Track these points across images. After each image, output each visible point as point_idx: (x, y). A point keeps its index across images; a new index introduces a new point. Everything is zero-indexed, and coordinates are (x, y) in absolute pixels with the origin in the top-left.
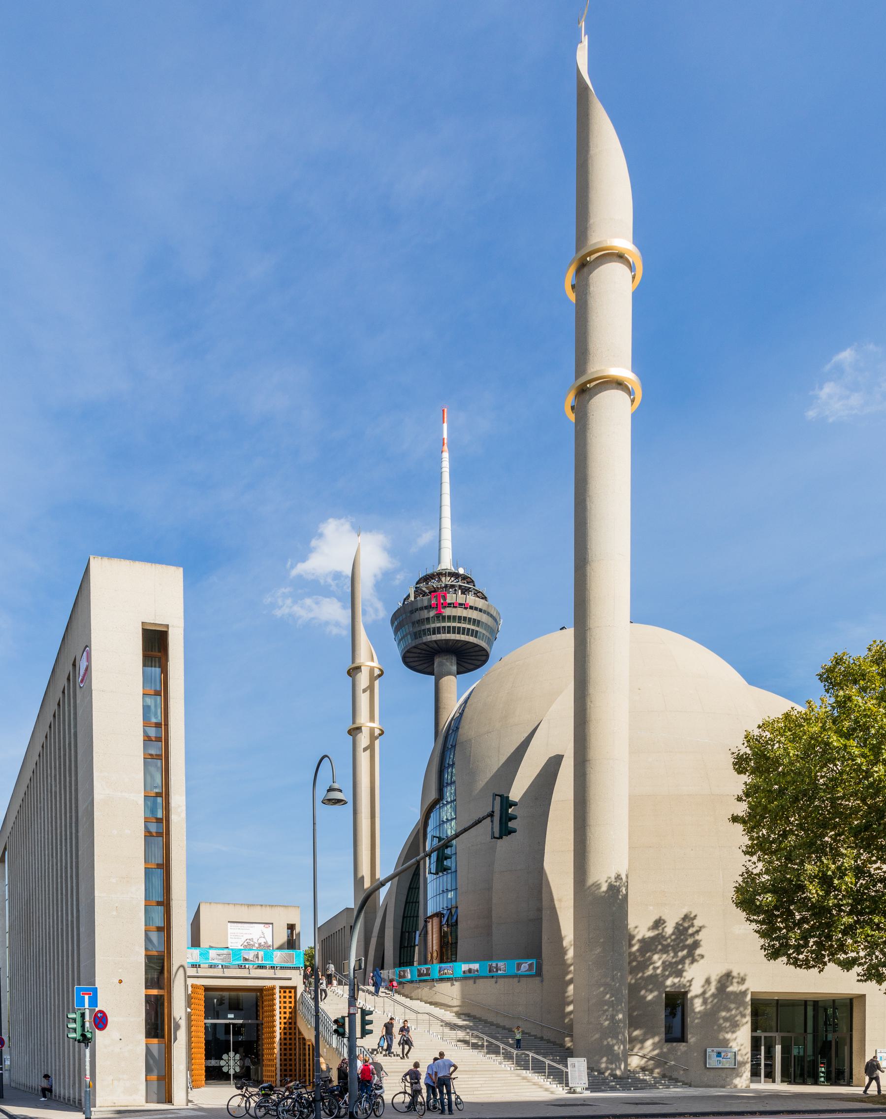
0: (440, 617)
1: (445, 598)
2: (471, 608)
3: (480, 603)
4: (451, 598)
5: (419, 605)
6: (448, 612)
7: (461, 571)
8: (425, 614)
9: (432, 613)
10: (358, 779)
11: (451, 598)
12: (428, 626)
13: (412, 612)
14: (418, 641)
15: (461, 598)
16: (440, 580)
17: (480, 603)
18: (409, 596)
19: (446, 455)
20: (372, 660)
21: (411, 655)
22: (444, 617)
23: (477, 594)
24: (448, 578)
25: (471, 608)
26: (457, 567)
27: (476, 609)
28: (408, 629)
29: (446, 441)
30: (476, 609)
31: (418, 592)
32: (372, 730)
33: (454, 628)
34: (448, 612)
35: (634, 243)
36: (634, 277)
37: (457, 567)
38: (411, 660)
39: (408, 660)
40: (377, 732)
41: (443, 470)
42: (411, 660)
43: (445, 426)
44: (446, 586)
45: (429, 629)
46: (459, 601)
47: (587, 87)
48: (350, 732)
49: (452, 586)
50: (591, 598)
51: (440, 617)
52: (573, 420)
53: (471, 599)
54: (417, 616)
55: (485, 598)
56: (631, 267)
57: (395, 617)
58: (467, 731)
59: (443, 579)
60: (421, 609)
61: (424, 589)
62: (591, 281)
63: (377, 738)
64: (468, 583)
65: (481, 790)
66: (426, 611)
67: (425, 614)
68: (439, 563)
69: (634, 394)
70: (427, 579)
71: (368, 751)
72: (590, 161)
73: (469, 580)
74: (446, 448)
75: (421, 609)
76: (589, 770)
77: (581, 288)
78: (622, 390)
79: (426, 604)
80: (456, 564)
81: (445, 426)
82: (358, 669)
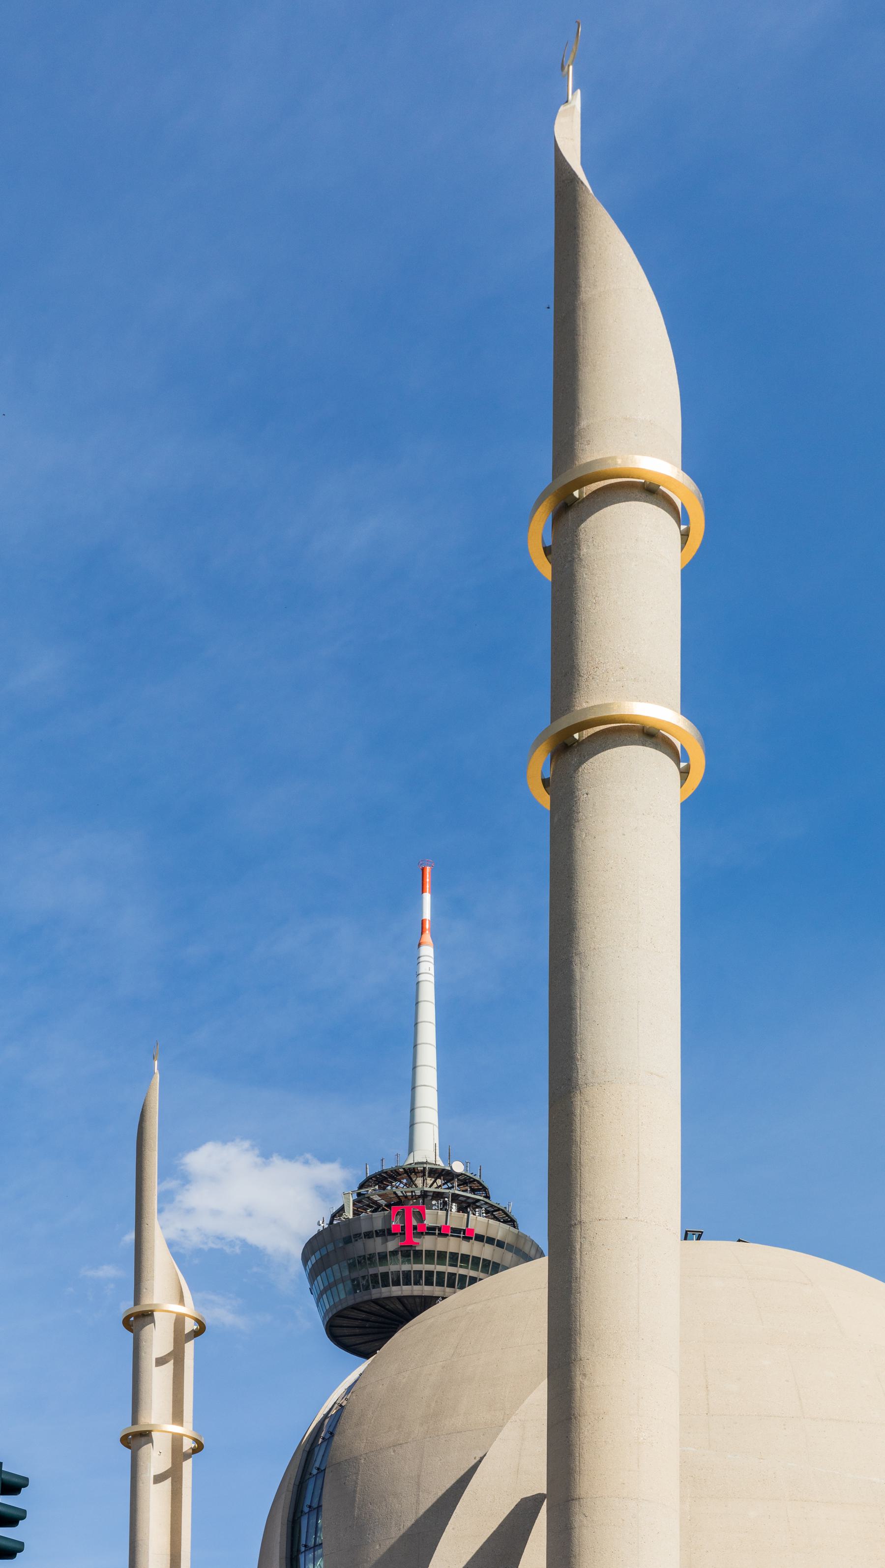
0: (409, 1253)
1: (421, 1216)
2: (480, 1238)
3: (499, 1230)
4: (433, 1217)
5: (365, 1228)
6: (427, 1243)
7: (458, 1167)
8: (377, 1245)
9: (392, 1245)
10: (141, 1535)
11: (433, 1217)
12: (382, 1269)
13: (348, 1240)
14: (361, 1296)
15: (455, 1218)
16: (411, 1183)
17: (499, 1230)
18: (342, 1209)
19: (427, 951)
20: (181, 1301)
21: (345, 1322)
22: (418, 1255)
23: (493, 1212)
24: (429, 1181)
25: (480, 1238)
26: (449, 1159)
27: (490, 1241)
28: (339, 1270)
29: (427, 926)
30: (490, 1241)
31: (362, 1203)
32: (177, 1440)
33: (441, 1274)
34: (427, 1243)
35: (685, 468)
36: (685, 536)
37: (449, 1159)
38: (346, 1331)
39: (338, 1331)
40: (188, 1445)
41: (422, 978)
42: (346, 1331)
43: (427, 897)
44: (424, 1194)
45: (385, 1275)
46: (452, 1224)
47: (573, 178)
48: (126, 1440)
49: (438, 1196)
50: (585, 1159)
51: (409, 1253)
52: (548, 806)
53: (479, 1222)
54: (359, 1248)
55: (510, 1221)
56: (679, 515)
57: (311, 1247)
58: (351, 1441)
59: (419, 1181)
60: (369, 1235)
61: (376, 1198)
62: (582, 536)
63: (187, 1456)
64: (473, 1191)
65: (379, 1562)
66: (379, 1240)
67: (377, 1245)
68: (411, 1149)
69: (687, 758)
70: (382, 1179)
71: (168, 1483)
72: (580, 313)
73: (475, 1186)
74: (427, 937)
75: (369, 1235)
76: (578, 1520)
77: (564, 552)
78: (656, 746)
79: (378, 1225)
80: (448, 1153)
81: (427, 897)
82: (147, 1316)
